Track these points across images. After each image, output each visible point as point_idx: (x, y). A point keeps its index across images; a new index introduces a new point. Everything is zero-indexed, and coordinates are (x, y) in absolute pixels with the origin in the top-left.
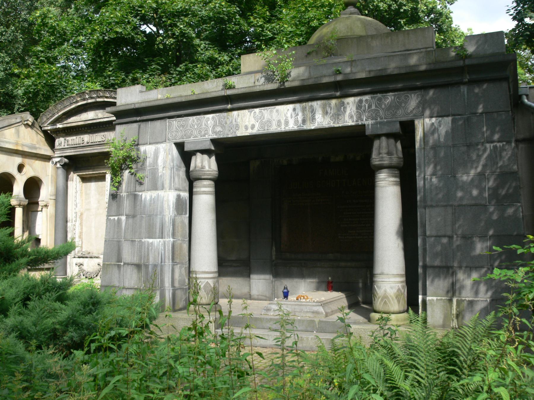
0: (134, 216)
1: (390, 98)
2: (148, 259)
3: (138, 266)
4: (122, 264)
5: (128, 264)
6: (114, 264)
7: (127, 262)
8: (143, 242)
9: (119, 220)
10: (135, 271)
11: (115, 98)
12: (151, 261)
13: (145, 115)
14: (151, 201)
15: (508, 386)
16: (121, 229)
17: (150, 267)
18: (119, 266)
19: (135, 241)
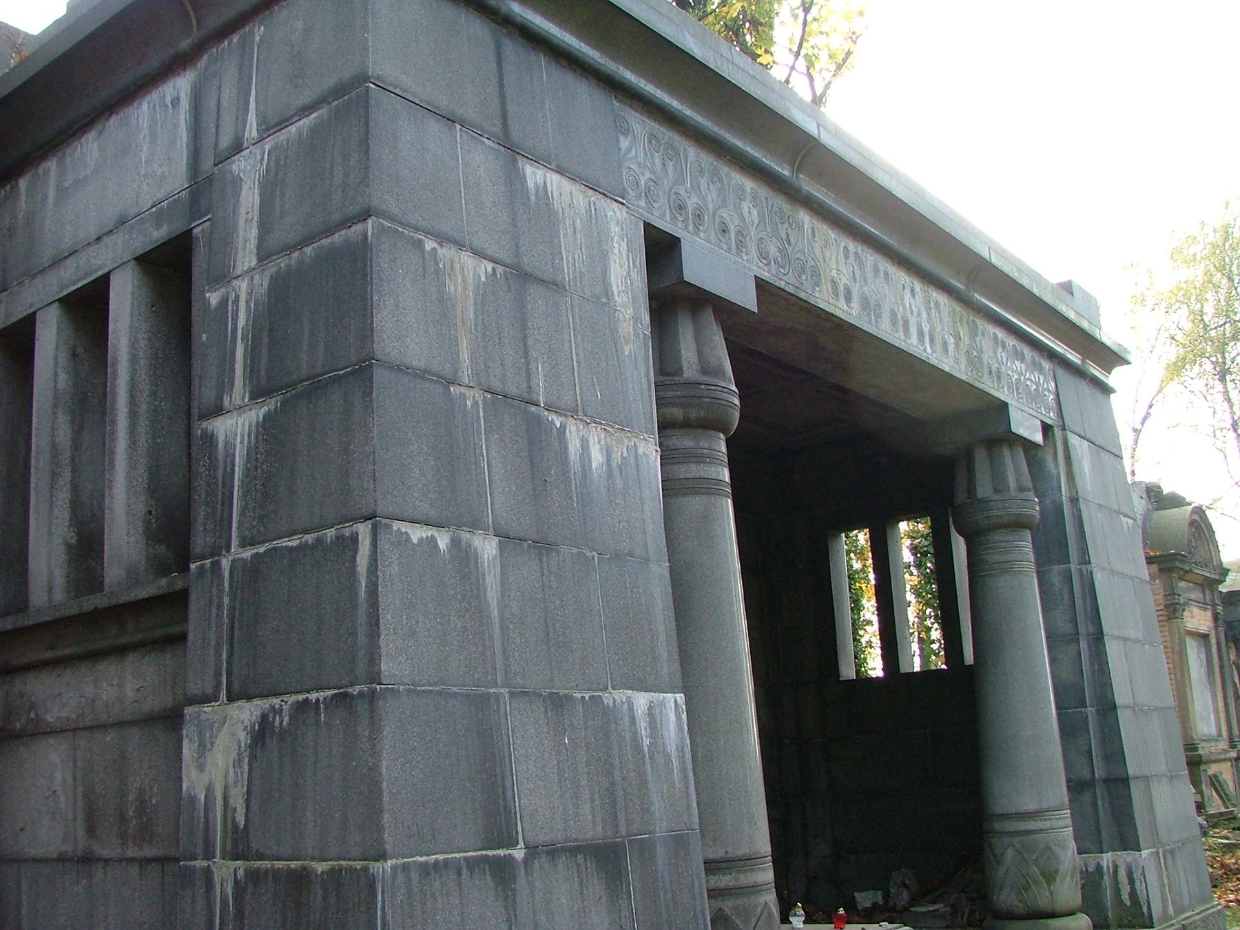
0: (543, 546)
1: (235, 39)
2: (645, 809)
3: (608, 858)
4: (519, 853)
5: (553, 852)
6: (472, 864)
7: (542, 838)
8: (606, 711)
9: (464, 556)
10: (596, 887)
11: (713, 893)
12: (661, 827)
13: (559, 25)
14: (610, 475)
15: (864, 566)
16: (481, 613)
17: (661, 851)
18: (502, 871)
19: (570, 698)
